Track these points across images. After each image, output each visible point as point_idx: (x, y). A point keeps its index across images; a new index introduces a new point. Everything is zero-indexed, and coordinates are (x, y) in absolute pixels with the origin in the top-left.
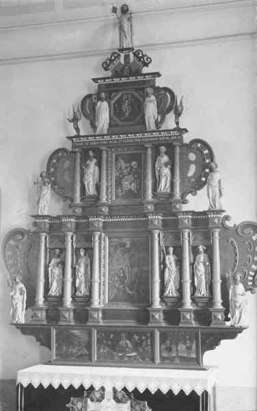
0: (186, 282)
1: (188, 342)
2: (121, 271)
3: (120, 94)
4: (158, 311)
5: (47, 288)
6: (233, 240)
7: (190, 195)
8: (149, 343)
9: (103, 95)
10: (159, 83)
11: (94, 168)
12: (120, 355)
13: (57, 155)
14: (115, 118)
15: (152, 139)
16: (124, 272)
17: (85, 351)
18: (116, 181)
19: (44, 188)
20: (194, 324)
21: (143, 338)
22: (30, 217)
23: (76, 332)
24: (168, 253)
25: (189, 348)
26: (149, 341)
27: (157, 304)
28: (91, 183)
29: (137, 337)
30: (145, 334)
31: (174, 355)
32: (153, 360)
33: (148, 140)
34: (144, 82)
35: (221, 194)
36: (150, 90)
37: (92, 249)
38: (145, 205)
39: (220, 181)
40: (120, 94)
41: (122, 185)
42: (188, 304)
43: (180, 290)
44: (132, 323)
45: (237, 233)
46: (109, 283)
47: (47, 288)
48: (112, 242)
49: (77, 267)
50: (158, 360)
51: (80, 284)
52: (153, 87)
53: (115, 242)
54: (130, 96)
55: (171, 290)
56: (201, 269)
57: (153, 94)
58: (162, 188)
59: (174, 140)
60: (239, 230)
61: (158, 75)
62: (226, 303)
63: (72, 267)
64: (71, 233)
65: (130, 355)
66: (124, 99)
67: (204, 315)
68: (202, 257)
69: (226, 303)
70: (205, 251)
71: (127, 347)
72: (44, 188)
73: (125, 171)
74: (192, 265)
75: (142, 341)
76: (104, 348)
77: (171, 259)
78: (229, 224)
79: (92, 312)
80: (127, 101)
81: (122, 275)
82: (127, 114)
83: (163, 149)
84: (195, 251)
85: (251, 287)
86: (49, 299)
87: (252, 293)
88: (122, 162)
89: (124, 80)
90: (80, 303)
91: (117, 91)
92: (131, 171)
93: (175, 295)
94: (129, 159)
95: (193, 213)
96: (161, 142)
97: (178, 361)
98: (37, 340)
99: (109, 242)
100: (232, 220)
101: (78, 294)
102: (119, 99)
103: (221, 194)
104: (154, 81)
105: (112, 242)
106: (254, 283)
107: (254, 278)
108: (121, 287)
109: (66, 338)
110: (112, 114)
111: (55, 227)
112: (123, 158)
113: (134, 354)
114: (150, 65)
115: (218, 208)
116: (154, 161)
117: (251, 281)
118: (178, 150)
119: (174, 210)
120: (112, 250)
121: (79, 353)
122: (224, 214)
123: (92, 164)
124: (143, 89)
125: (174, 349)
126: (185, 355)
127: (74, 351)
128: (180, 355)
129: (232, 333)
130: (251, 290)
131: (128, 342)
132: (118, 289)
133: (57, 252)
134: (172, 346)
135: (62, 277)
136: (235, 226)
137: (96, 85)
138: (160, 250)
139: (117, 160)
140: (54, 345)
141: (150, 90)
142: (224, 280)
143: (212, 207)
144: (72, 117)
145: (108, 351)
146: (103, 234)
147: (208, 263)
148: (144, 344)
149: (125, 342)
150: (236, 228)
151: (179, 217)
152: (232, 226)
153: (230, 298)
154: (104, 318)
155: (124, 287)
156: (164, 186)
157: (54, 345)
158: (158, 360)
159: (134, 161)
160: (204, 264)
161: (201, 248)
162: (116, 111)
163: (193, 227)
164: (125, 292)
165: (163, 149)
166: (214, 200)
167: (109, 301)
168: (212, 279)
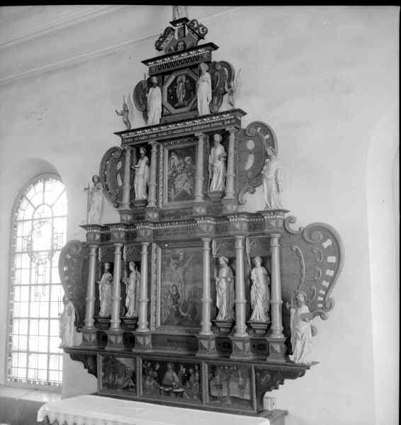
0: (205, 302)
1: (241, 379)
2: (174, 287)
3: (173, 77)
4: (206, 338)
5: (249, 311)
6: (297, 247)
7: (247, 194)
8: (197, 378)
9: (155, 80)
10: (216, 56)
11: (145, 167)
12: (167, 389)
13: (112, 156)
14: (168, 105)
15: (202, 127)
16: (177, 290)
17: (132, 384)
18: (169, 181)
19: (96, 194)
20: (250, 357)
21: (191, 371)
22: (80, 228)
23: (122, 360)
24: (253, 266)
25: (242, 387)
26: (197, 375)
27: (206, 330)
28: (141, 184)
29: (184, 369)
30: (192, 366)
31: (225, 394)
32: (200, 397)
33: (198, 128)
34: (197, 58)
35: (278, 191)
36: (204, 67)
37: (270, 257)
38: (225, 205)
39: (277, 171)
40: (173, 77)
41: (174, 185)
42: (241, 330)
43: (269, 313)
44: (181, 351)
45: (303, 238)
46: (161, 303)
47: (249, 311)
48: (165, 254)
49: (217, 279)
50: (206, 399)
51: (130, 303)
52: (208, 62)
53: (168, 253)
54: (184, 78)
55: (259, 314)
56: (223, 285)
57: (207, 71)
58: (214, 186)
59: (228, 125)
60: (305, 235)
61: (215, 48)
62: (287, 331)
63: (121, 281)
64: (209, 239)
65: (178, 390)
66: (178, 82)
67: (261, 347)
68: (225, 271)
69: (287, 331)
70: (263, 265)
71: (174, 381)
72: (96, 194)
73: (178, 169)
74: (213, 281)
75: (189, 375)
76: (150, 380)
77: (258, 273)
78: (294, 227)
79: (203, 342)
80: (181, 84)
81: (175, 293)
82: (181, 99)
83: (218, 138)
84: (216, 264)
85: (321, 311)
86: (99, 320)
87: (323, 319)
88: (175, 157)
89: (176, 58)
90: (129, 326)
91: (170, 73)
92: (184, 167)
93: (264, 321)
94: (182, 153)
95: (251, 215)
96: (214, 129)
97: (229, 402)
98: (85, 367)
99: (162, 254)
100: (297, 223)
101: (219, 318)
102: (172, 83)
103: (278, 191)
104: (210, 56)
105: (165, 254)
106: (324, 305)
107: (325, 298)
108: (174, 307)
109: (112, 366)
110: (166, 99)
111: (105, 234)
112: (176, 153)
113: (181, 390)
114: (205, 37)
115: (274, 207)
116: (207, 153)
117: (321, 302)
118: (232, 137)
119: (224, 212)
120: (165, 263)
121: (125, 385)
122: (287, 215)
123: (219, 150)
124: (196, 66)
125: (225, 388)
126: (237, 396)
127: (120, 381)
128: (231, 395)
129: (296, 372)
130: (320, 314)
131: (175, 374)
132: (171, 310)
133: (107, 266)
134: (222, 384)
135: (268, 298)
136: (300, 229)
137: (146, 69)
138: (245, 263)
139: (170, 155)
140: (101, 373)
141: (204, 67)
142: (285, 299)
143: (267, 206)
144: (120, 109)
145: (154, 384)
146: (154, 245)
147: (229, 280)
148: (191, 378)
149: (171, 375)
150: (302, 232)
151: (230, 220)
152: (297, 230)
153: (291, 326)
154: (154, 343)
155: (177, 308)
156: (216, 185)
157: (101, 373)
158: (206, 399)
159: (189, 155)
160: (226, 278)
161: (223, 261)
162: (172, 98)
163: (248, 233)
164: (178, 314)
165: (218, 138)
166: (269, 197)
167: (161, 323)
168: (270, 298)
